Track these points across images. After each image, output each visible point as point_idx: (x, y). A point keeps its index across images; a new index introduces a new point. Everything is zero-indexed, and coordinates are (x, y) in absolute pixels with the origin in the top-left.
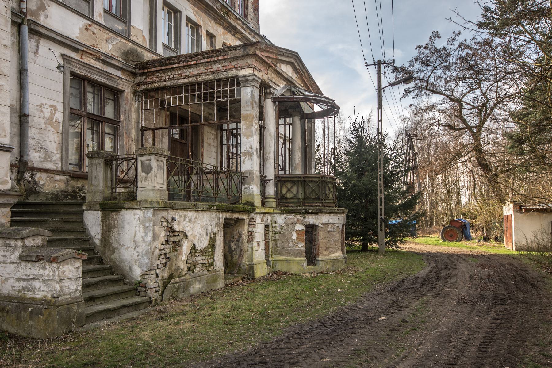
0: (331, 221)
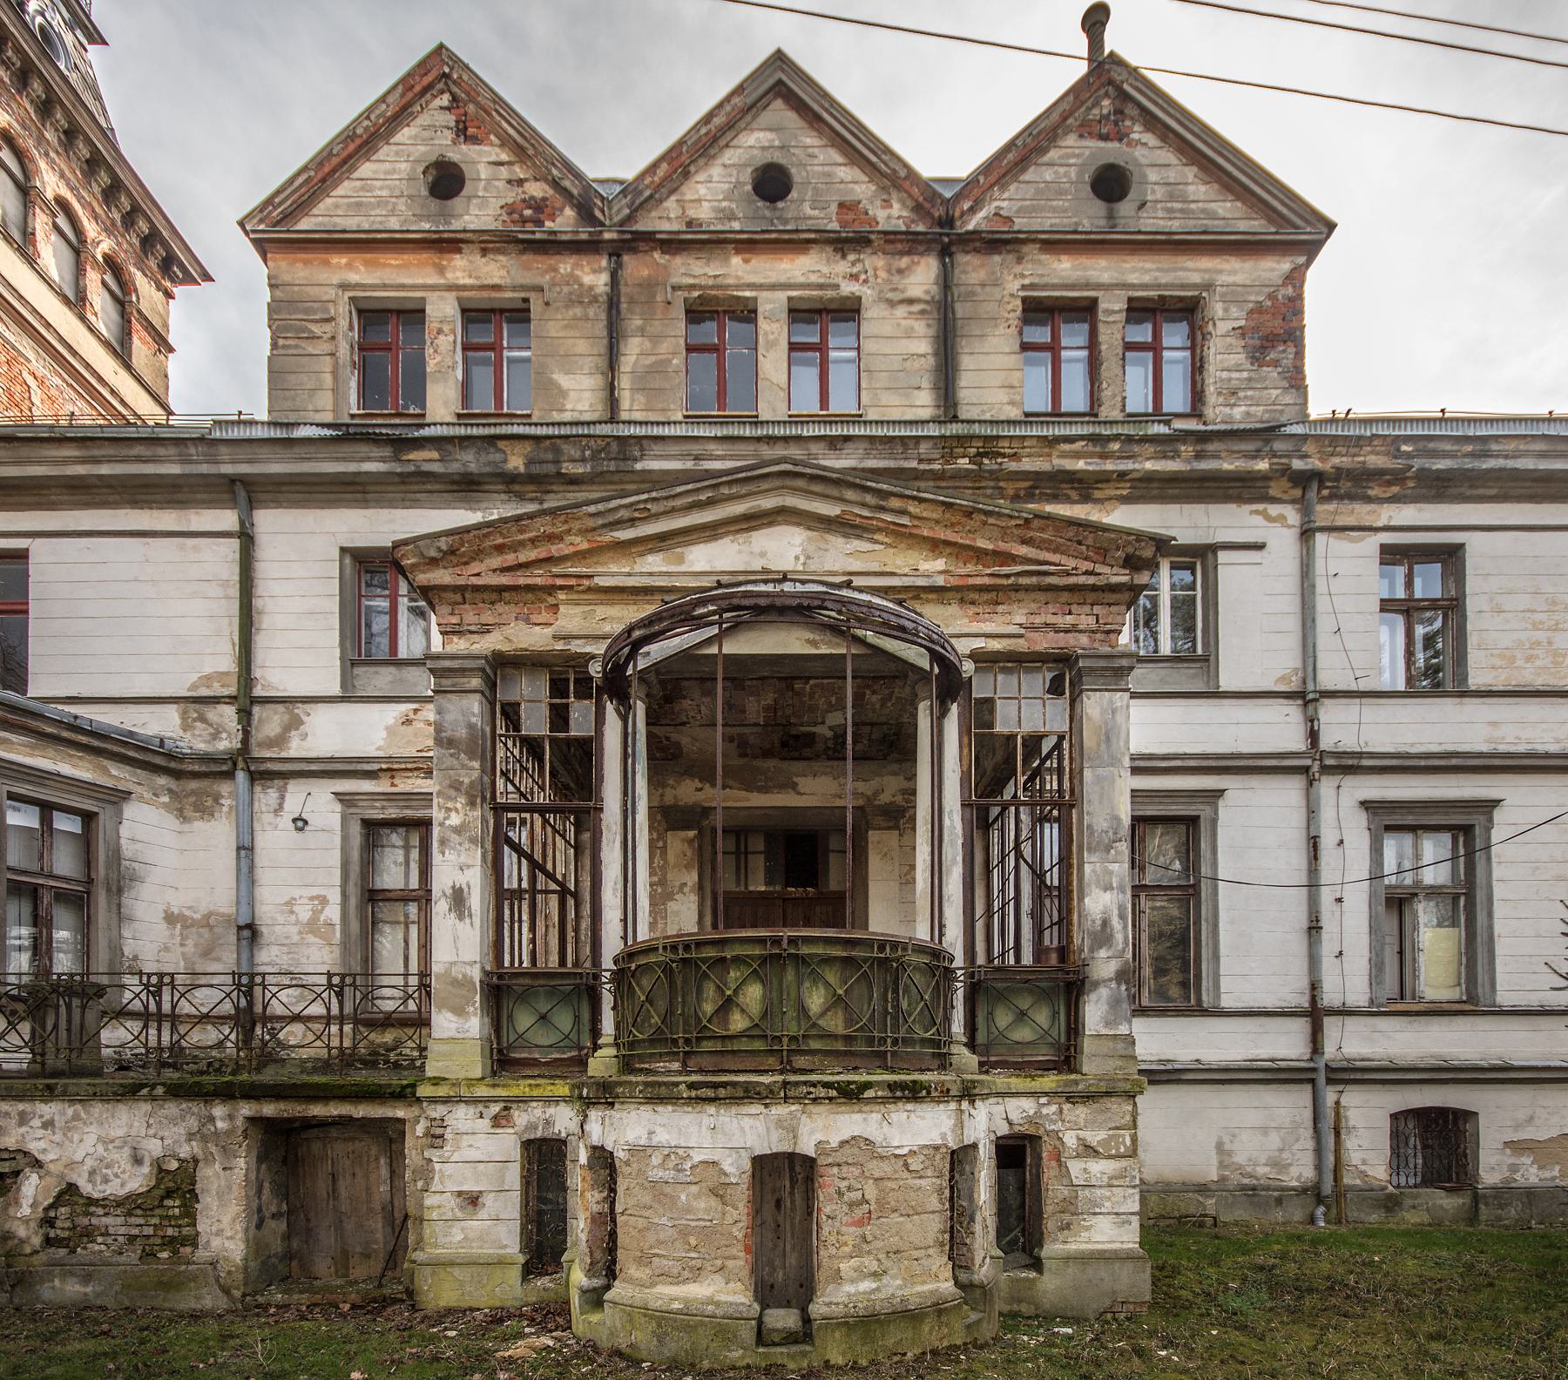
0: (662, 1137)
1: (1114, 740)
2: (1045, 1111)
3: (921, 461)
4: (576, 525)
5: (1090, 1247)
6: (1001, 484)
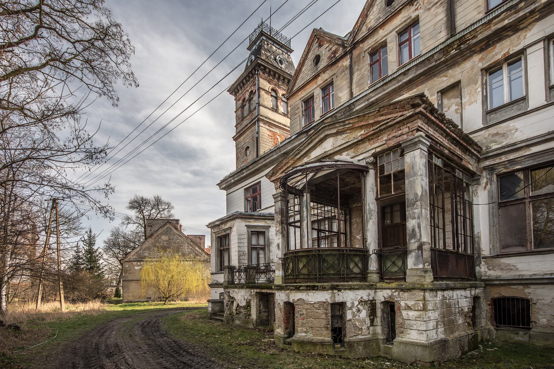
1: (415, 167)
2: (394, 294)
3: (436, 61)
4: (290, 159)
5: (410, 340)
6: (473, 49)
